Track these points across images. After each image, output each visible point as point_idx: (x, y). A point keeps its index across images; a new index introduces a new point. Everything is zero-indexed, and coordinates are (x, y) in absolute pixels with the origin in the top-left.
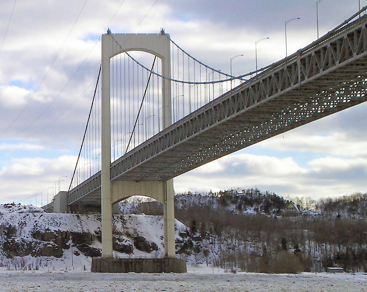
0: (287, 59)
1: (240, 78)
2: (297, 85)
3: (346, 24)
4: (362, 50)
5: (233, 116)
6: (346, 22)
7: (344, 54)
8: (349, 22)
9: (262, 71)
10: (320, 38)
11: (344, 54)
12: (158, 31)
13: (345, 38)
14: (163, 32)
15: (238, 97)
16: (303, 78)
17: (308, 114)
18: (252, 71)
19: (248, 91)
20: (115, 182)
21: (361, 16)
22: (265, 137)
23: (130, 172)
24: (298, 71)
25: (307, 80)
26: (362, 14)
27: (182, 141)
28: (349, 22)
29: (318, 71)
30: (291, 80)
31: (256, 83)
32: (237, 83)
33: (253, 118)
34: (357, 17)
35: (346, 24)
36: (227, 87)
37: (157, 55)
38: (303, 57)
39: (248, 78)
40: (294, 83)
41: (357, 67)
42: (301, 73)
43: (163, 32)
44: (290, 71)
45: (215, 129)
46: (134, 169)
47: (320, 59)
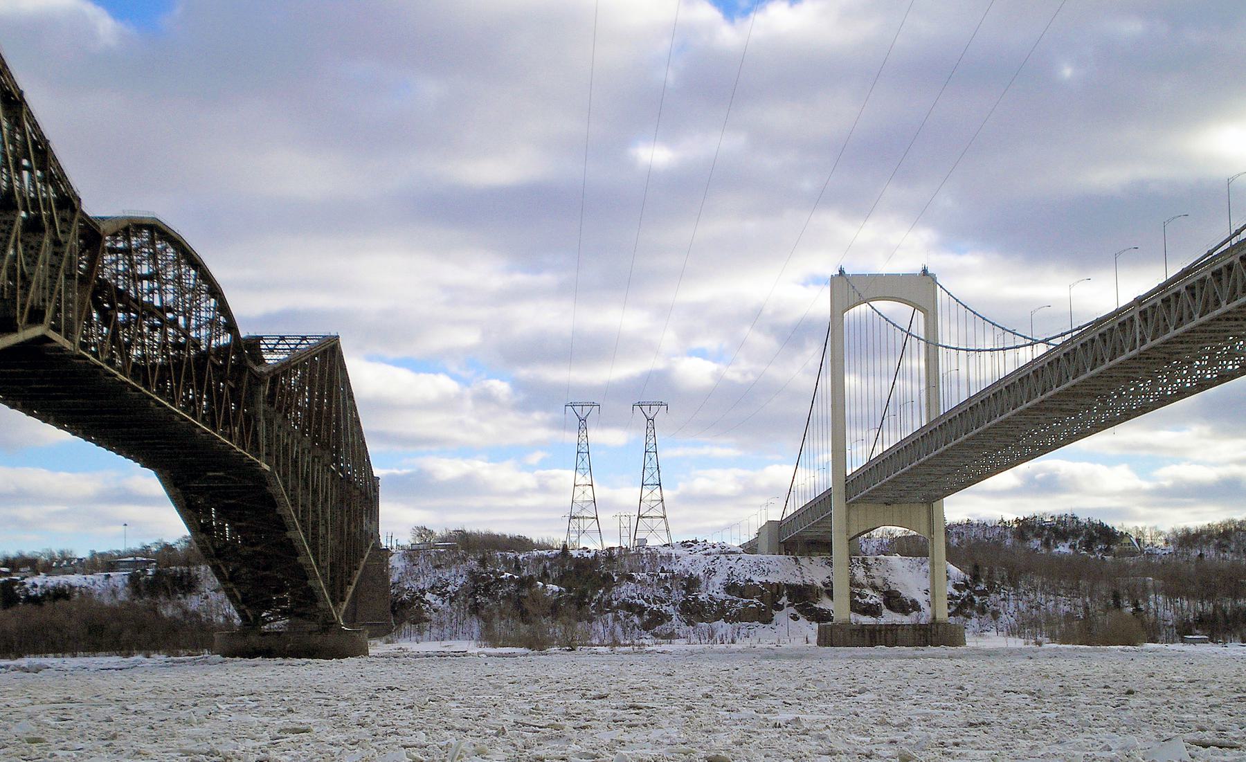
0: (1118, 312)
1: (1046, 341)
3: (1210, 256)
5: (1035, 401)
6: (1210, 253)
8: (1214, 254)
9: (1080, 331)
17: (1152, 397)
21: (1233, 244)
25: (1149, 344)
26: (1234, 241)
28: (1214, 254)
30: (1125, 344)
32: (1041, 349)
35: (1210, 256)
36: (1026, 355)
38: (1143, 308)
39: (1058, 341)
42: (1140, 332)
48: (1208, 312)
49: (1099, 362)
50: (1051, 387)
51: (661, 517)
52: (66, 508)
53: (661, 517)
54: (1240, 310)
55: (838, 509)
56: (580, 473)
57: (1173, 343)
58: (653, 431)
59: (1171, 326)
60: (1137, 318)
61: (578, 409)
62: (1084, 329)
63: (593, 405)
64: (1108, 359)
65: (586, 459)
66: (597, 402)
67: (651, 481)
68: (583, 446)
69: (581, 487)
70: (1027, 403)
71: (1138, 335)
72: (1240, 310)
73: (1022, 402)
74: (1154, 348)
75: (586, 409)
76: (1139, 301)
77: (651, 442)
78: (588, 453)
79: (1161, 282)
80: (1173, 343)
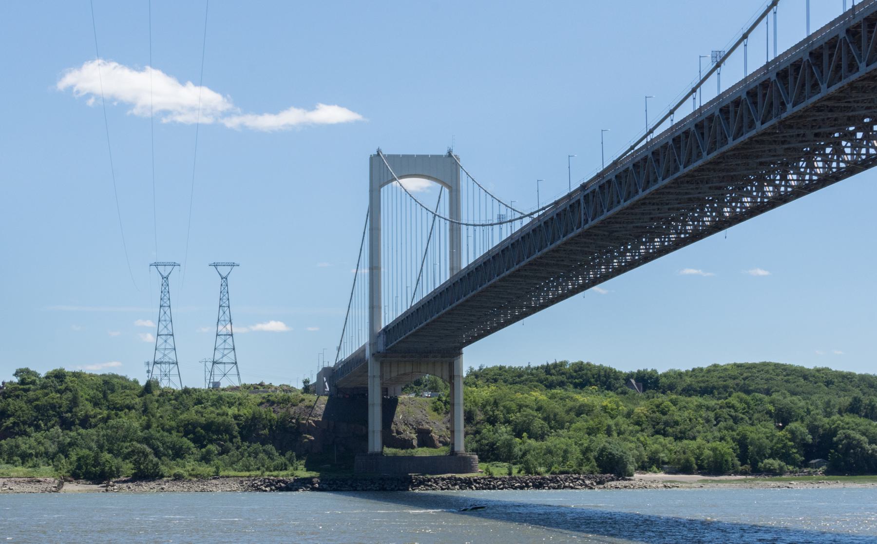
0: (569, 196)
1: (529, 215)
2: (580, 230)
3: (632, 151)
4: (741, 133)
5: (512, 270)
6: (632, 148)
7: (838, 67)
8: (636, 148)
9: (544, 211)
10: (751, 72)
11: (838, 67)
12: (444, 153)
13: (805, 60)
14: (450, 155)
15: (594, 196)
16: (586, 221)
17: (667, 240)
18: (533, 211)
19: (687, 137)
20: (120, 489)
21: (648, 140)
22: (563, 296)
23: (400, 342)
24: (581, 210)
25: (591, 223)
26: (649, 138)
27: (490, 283)
28: (636, 148)
29: (677, 169)
30: (680, 161)
31: (661, 147)
32: (527, 221)
33: (588, 247)
34: (644, 142)
35: (632, 151)
36: (517, 226)
37: (444, 183)
38: (586, 193)
39: (536, 216)
40: (793, 104)
41: (652, 207)
42: (584, 214)
43: (450, 155)
44: (573, 212)
45: (494, 286)
46: (407, 338)
47: (728, 123)
48: (742, 135)
49: (615, 203)
50: (602, 211)
51: (233, 363)
52: (259, 327)
53: (233, 363)
54: (653, 196)
55: (373, 369)
56: (163, 324)
57: (663, 193)
58: (226, 288)
59: (704, 151)
60: (582, 201)
61: (161, 268)
62: (547, 209)
63: (174, 265)
64: (661, 178)
65: (227, 313)
66: (177, 262)
67: (165, 332)
68: (165, 301)
69: (163, 337)
70: (551, 244)
71: (582, 216)
72: (653, 196)
73: (547, 245)
74: (595, 227)
75: (169, 268)
76: (584, 187)
77: (224, 298)
78: (229, 307)
79: (599, 172)
80: (663, 193)
